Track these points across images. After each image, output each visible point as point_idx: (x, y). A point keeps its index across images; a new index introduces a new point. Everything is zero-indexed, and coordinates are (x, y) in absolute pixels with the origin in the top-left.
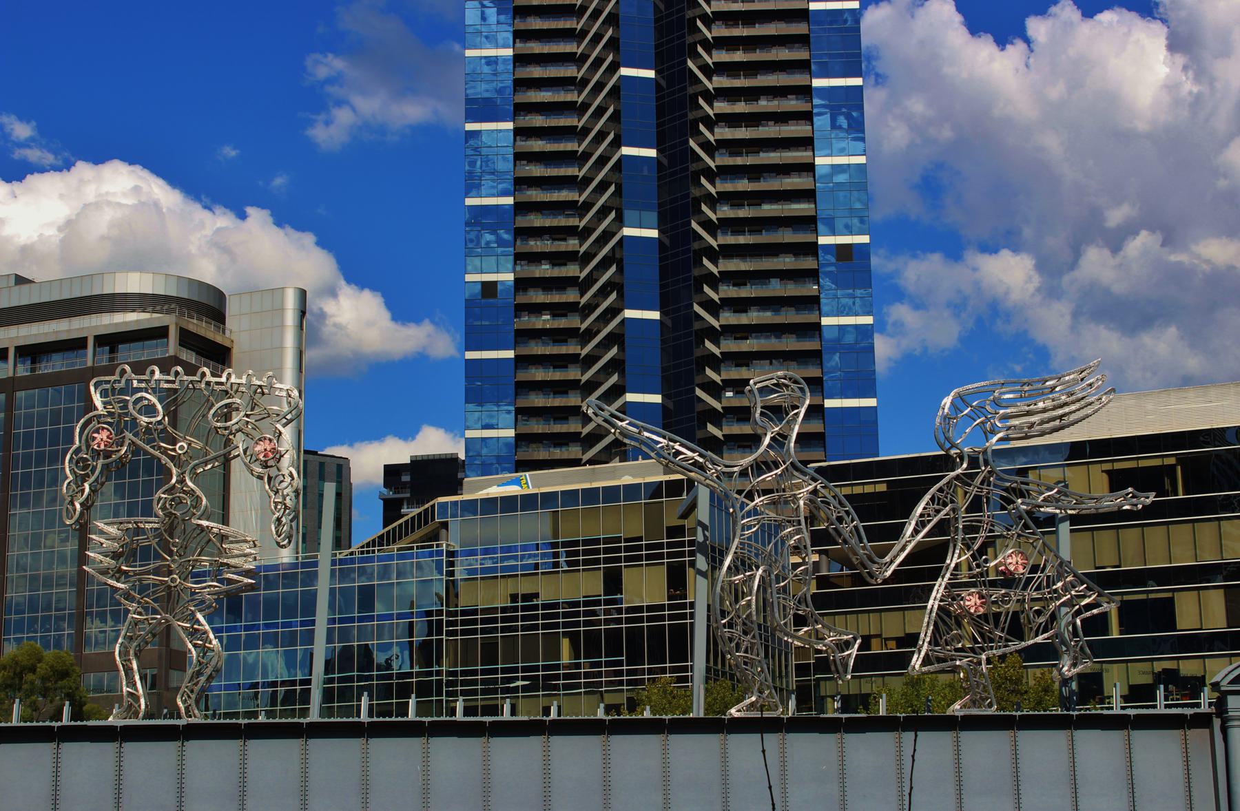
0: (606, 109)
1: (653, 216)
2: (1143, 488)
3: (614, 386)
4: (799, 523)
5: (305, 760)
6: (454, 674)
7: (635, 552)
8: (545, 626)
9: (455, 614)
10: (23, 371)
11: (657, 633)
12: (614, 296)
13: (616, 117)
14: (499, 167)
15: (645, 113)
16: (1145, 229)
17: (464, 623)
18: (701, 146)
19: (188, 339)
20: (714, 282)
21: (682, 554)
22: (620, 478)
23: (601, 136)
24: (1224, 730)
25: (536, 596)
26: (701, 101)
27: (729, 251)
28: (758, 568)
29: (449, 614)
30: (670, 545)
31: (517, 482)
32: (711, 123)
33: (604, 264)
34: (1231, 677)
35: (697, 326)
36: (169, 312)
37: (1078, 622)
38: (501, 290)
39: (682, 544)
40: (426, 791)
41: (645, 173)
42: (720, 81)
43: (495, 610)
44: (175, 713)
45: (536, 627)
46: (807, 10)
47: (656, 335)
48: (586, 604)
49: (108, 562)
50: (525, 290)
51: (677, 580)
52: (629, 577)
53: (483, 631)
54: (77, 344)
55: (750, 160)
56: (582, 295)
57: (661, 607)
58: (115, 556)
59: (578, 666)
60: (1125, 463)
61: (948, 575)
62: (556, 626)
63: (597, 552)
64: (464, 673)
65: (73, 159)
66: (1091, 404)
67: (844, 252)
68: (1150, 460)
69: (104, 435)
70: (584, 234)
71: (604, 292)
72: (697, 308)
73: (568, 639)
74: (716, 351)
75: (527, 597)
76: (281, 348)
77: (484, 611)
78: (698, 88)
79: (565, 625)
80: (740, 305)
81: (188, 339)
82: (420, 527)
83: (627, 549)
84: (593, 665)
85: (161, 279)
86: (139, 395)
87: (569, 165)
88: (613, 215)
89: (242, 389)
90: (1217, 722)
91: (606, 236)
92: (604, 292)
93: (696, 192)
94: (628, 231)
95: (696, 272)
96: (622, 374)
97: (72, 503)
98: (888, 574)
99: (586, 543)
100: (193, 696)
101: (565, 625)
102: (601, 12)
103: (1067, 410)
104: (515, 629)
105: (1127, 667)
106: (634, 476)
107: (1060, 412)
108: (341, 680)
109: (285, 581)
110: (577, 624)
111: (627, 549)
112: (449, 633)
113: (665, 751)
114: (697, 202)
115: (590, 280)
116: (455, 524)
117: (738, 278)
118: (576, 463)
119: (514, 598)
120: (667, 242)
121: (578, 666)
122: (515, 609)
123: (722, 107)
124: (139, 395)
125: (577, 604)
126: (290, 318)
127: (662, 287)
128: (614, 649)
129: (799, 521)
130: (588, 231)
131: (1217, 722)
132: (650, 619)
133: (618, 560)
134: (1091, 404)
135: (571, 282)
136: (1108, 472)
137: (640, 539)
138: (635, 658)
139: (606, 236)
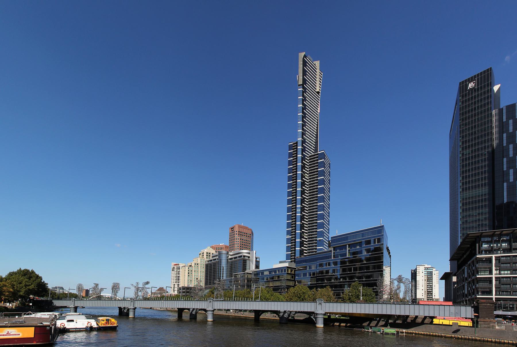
2: (317, 158)
14: (292, 282)
16: (48, 330)
38: (289, 266)
65: (452, 301)
73: (473, 309)
105: (337, 311)
109: (358, 267)
113: (287, 303)
129: (211, 284)
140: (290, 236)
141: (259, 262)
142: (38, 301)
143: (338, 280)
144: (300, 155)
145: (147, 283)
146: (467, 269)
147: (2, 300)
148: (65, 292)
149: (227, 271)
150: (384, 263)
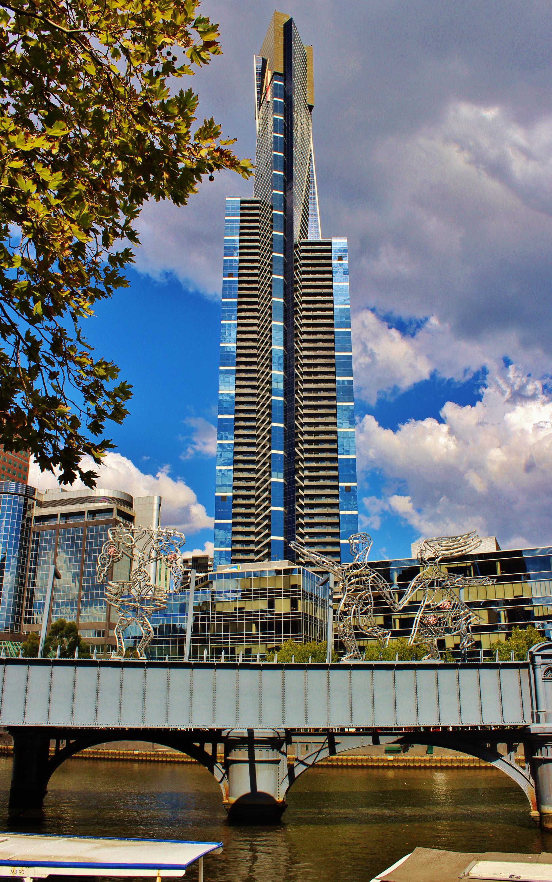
0: (266, 437)
1: (282, 475)
3: (267, 534)
4: (368, 589)
5: (192, 677)
6: (213, 636)
7: (280, 594)
8: (246, 619)
9: (214, 614)
10: (63, 522)
11: (286, 623)
12: (268, 502)
13: (270, 440)
15: (279, 439)
17: (217, 617)
18: (299, 450)
19: (120, 513)
20: (302, 497)
21: (296, 595)
22: (273, 566)
23: (264, 446)
24: (534, 669)
25: (244, 608)
26: (299, 435)
27: (308, 487)
28: (353, 605)
29: (212, 614)
30: (292, 591)
31: (236, 567)
32: (302, 443)
33: (265, 490)
34: (537, 649)
35: (297, 513)
36: (113, 503)
37: (470, 627)
39: (296, 591)
40: (237, 691)
41: (279, 459)
42: (306, 428)
43: (228, 613)
44: (136, 657)
45: (236, 620)
46: (336, 405)
47: (282, 517)
48: (262, 612)
49: (113, 597)
50: (236, 499)
51: (294, 604)
52: (277, 602)
53: (224, 621)
54: (82, 514)
55: (316, 456)
56: (256, 501)
57: (288, 614)
58: (116, 594)
59: (258, 634)
60: (453, 565)
61: (422, 609)
62: (251, 619)
63: (266, 593)
64: (217, 635)
66: (472, 546)
67: (348, 488)
68: (462, 564)
69: (113, 549)
70: (257, 480)
71: (264, 500)
72: (297, 507)
74: (303, 522)
75: (240, 609)
76: (152, 517)
77: (225, 613)
78: (298, 431)
79: (254, 619)
80: (312, 506)
81: (120, 513)
82: (202, 582)
83: (277, 592)
84: (263, 634)
85: (112, 491)
86: (126, 535)
87: (253, 456)
88: (268, 474)
89: (164, 534)
90: (531, 666)
91: (265, 481)
92: (264, 500)
93: (297, 466)
94: (273, 479)
95: (296, 494)
96: (270, 529)
97: (100, 574)
98: (401, 608)
99: (262, 590)
100: (143, 649)
101: (254, 619)
102: (265, 404)
103: (464, 548)
104: (228, 620)
106: (278, 566)
107: (462, 549)
108: (159, 637)
110: (258, 619)
111: (277, 592)
112: (212, 621)
114: (297, 470)
115: (259, 496)
116: (215, 583)
117: (311, 497)
118: (252, 561)
119: (235, 609)
120: (287, 484)
121: (258, 634)
122: (236, 613)
123: (306, 437)
124: (126, 535)
125: (258, 612)
126: (156, 506)
127: (284, 499)
128: (271, 628)
130: (258, 479)
131: (531, 666)
132: (284, 618)
133: (273, 596)
134: (472, 546)
135: (252, 497)
136: (447, 568)
137: (281, 589)
138: (279, 632)
139: (265, 481)
140: (224, 347)
141: (358, 729)
142: (6, 370)
143: (78, 482)
144: (341, 432)
145: (210, 60)
146: (230, 197)
147: (121, 191)
148: (474, 757)
149: (21, 538)
150: (4, 577)
